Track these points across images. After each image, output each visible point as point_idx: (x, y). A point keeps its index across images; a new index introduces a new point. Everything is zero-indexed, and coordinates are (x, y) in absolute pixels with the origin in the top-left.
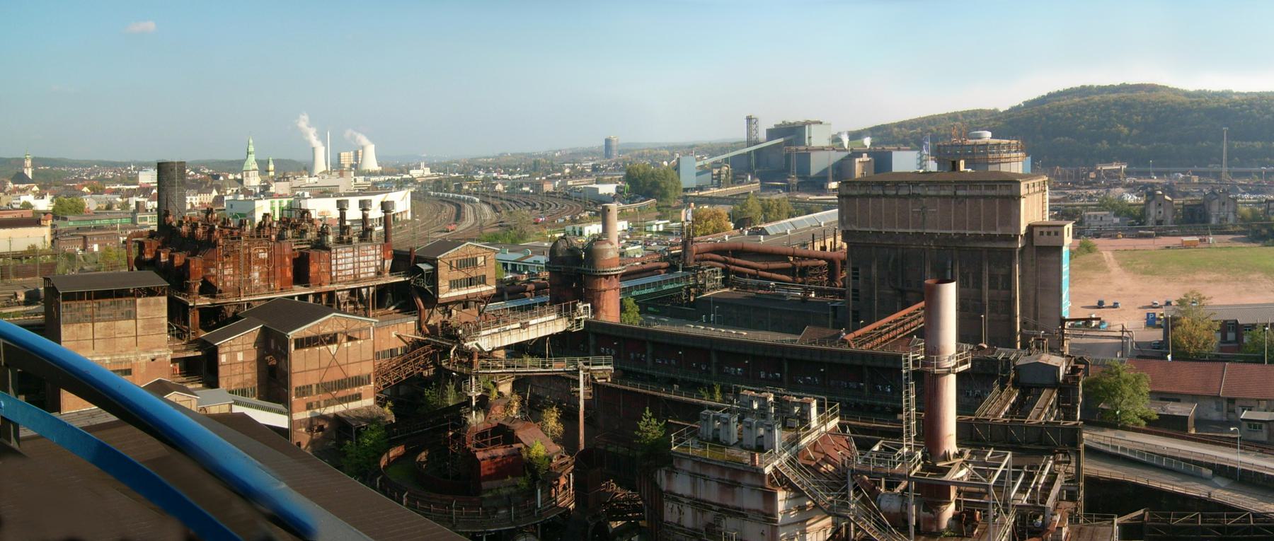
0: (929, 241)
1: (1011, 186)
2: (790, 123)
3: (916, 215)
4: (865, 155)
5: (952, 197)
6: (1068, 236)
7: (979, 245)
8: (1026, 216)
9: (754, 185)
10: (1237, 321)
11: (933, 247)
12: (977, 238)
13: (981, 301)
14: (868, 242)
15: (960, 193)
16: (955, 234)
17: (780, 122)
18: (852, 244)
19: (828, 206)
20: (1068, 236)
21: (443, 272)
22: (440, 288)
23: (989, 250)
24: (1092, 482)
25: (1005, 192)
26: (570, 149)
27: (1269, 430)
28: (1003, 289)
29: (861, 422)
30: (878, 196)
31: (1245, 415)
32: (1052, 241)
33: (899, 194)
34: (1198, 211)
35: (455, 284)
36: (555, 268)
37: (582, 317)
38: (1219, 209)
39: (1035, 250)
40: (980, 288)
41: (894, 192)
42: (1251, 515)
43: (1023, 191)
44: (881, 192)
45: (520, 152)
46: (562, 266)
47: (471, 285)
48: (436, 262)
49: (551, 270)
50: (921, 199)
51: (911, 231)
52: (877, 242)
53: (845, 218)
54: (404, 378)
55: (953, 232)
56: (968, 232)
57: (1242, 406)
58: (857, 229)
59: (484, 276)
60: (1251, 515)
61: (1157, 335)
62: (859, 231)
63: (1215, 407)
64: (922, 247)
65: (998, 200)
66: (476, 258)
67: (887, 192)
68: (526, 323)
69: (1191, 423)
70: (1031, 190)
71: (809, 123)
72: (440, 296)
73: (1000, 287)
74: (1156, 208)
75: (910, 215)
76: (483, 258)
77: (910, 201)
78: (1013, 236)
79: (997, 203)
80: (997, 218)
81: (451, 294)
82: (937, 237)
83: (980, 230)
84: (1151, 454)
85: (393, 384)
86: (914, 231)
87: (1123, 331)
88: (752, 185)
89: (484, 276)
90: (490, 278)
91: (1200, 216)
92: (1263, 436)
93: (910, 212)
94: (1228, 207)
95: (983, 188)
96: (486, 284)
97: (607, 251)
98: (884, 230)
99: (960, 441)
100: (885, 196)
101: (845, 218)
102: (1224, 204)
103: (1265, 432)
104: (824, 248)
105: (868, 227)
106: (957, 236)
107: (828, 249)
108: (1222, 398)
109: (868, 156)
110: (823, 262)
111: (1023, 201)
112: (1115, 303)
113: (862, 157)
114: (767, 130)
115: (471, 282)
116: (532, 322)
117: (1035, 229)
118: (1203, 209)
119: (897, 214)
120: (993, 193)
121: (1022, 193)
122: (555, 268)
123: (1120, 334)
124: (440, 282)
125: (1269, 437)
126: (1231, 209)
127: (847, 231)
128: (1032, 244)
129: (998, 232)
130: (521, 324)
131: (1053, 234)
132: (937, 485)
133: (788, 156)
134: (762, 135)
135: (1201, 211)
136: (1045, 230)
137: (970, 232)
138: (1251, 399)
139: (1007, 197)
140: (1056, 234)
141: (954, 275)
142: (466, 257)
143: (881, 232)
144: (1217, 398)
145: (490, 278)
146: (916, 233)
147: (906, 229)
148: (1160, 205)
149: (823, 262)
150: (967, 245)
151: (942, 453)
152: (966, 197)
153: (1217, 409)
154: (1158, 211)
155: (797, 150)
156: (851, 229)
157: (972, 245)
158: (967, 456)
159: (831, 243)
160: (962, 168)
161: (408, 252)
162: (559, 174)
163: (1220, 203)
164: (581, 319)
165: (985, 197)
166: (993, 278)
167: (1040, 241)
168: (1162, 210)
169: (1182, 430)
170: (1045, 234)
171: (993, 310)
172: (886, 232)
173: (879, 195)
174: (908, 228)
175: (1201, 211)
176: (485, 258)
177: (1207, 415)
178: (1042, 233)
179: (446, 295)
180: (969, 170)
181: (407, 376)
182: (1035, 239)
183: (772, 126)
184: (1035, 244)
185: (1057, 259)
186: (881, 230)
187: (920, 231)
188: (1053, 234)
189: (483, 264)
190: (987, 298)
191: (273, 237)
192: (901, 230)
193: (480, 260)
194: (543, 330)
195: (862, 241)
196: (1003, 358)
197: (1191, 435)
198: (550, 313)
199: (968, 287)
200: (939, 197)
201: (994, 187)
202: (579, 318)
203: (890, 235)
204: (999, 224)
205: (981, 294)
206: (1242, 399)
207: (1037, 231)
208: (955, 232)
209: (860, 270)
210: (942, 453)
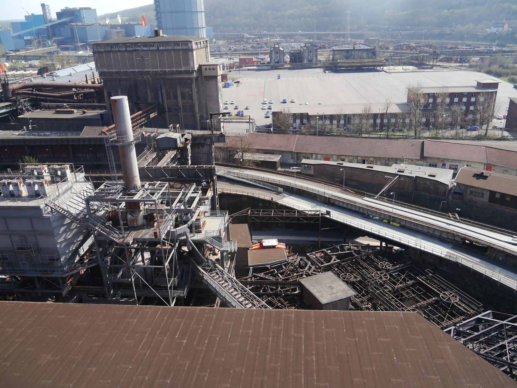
2: (70, 9)
3: (138, 61)
4: (119, 28)
8: (197, 60)
9: (53, 47)
10: (308, 113)
11: (150, 79)
12: (172, 73)
13: (178, 106)
14: (114, 78)
15: (161, 48)
16: (160, 71)
19: (83, 60)
24: (222, 196)
25: (185, 47)
27: (314, 169)
28: (189, 99)
31: (304, 161)
34: (298, 56)
38: (308, 55)
40: (177, 99)
41: (124, 49)
42: (296, 211)
44: (117, 49)
51: (136, 70)
52: (119, 77)
53: (99, 64)
55: (159, 70)
57: (304, 157)
58: (107, 71)
60: (296, 211)
61: (269, 121)
63: (291, 157)
64: (144, 79)
65: (181, 51)
67: (121, 49)
69: (278, 164)
70: (199, 46)
73: (187, 98)
74: (275, 54)
77: (134, 54)
78: (191, 71)
79: (181, 53)
82: (151, 73)
84: (255, 181)
87: (249, 119)
88: (52, 47)
91: (299, 59)
92: (312, 172)
94: (313, 54)
98: (122, 71)
99: (142, 179)
100: (119, 51)
101: (99, 64)
102: (310, 52)
103: (312, 170)
104: (94, 83)
106: (162, 72)
107: (97, 82)
108: (294, 152)
110: (92, 90)
111: (195, 52)
112: (284, 100)
113: (117, 29)
117: (202, 67)
118: (300, 55)
120: (178, 48)
123: (248, 121)
125: (314, 172)
126: (314, 55)
128: (202, 75)
129: (183, 69)
131: (212, 69)
134: (54, 16)
135: (299, 56)
136: (208, 67)
137: (168, 70)
138: (309, 153)
139: (186, 50)
140: (214, 69)
141: (163, 93)
144: (291, 152)
146: (140, 71)
148: (277, 53)
149: (92, 90)
150: (168, 77)
151: (133, 186)
152: (164, 50)
153: (292, 158)
154: (276, 56)
155: (77, 25)
156: (103, 71)
157: (170, 77)
158: (146, 186)
160: (161, 34)
163: (308, 51)
165: (174, 50)
166: (168, 94)
167: (206, 73)
168: (278, 55)
169: (274, 169)
171: (185, 111)
172: (123, 72)
175: (299, 56)
177: (287, 161)
178: (206, 69)
180: (165, 35)
182: (203, 72)
183: (59, 11)
185: (215, 82)
186: (120, 71)
188: (212, 69)
190: (181, 104)
192: (131, 70)
197: (278, 171)
199: (171, 99)
200: (150, 50)
202: (22, 290)
203: (126, 73)
205: (177, 102)
206: (304, 153)
207: (203, 68)
208: (160, 70)
209: (112, 93)
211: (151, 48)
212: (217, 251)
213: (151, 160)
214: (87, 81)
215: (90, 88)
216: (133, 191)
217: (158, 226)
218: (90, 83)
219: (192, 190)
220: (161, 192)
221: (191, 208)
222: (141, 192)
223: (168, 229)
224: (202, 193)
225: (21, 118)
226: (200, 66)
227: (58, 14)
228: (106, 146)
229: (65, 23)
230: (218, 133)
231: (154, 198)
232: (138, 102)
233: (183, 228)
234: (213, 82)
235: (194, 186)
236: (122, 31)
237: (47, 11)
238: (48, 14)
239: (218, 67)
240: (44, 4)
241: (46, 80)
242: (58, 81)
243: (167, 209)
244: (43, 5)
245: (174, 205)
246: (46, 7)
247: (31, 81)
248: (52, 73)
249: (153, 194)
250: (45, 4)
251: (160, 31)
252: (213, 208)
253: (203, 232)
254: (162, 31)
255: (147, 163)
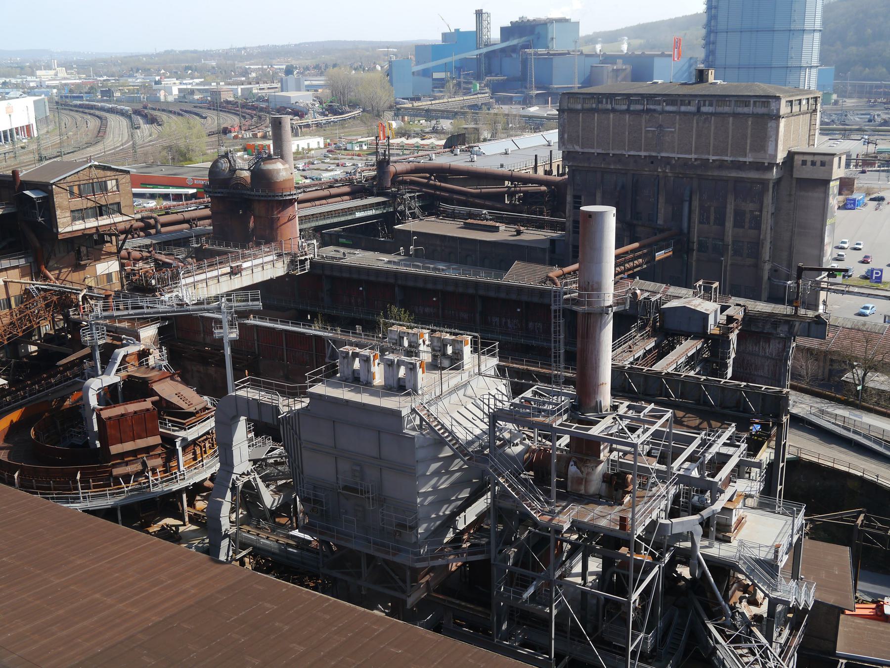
0: (665, 167)
1: (768, 102)
2: (528, 20)
3: (650, 135)
4: (619, 61)
5: (693, 114)
6: (839, 167)
7: (725, 173)
8: (785, 141)
11: (670, 175)
12: (722, 165)
14: (592, 165)
15: (705, 109)
16: (696, 159)
17: (516, 19)
18: (574, 168)
20: (839, 167)
21: (61, 199)
22: (58, 220)
23: (737, 180)
25: (761, 110)
26: (259, 47)
29: (541, 368)
30: (606, 111)
32: (818, 173)
33: (631, 109)
35: (79, 214)
36: (216, 193)
37: (307, 257)
39: (794, 182)
41: (625, 107)
43: (784, 109)
45: (192, 49)
46: (225, 191)
47: (101, 215)
48: (50, 188)
49: (211, 195)
50: (657, 115)
51: (643, 154)
53: (566, 136)
54: (20, 334)
56: (712, 158)
59: (118, 204)
62: (583, 153)
64: (656, 173)
66: (105, 182)
68: (237, 266)
71: (551, 21)
72: (60, 230)
73: (747, 225)
75: (643, 135)
76: (114, 182)
77: (645, 117)
80: (749, 141)
81: (76, 228)
83: (727, 156)
85: (6, 342)
86: (646, 154)
89: (118, 204)
90: (126, 206)
93: (643, 132)
95: (733, 103)
96: (121, 214)
97: (278, 171)
98: (611, 152)
100: (613, 110)
101: (566, 136)
105: (593, 148)
107: (555, 172)
109: (624, 63)
110: (543, 188)
111: (782, 122)
113: (615, 63)
114: (442, 34)
115: (100, 211)
116: (245, 265)
117: (796, 157)
119: (627, 133)
120: (746, 110)
121: (782, 113)
122: (216, 193)
124: (58, 212)
127: (569, 152)
128: (792, 175)
129: (749, 159)
130: (231, 268)
132: (587, 440)
133: (525, 63)
134: (495, 35)
137: (715, 158)
140: (823, 164)
141: (693, 208)
142: (91, 181)
143: (609, 154)
145: (126, 206)
146: (650, 157)
147: (638, 151)
149: (543, 188)
150: (710, 174)
151: (593, 404)
152: (712, 114)
157: (716, 173)
158: (622, 410)
159: (558, 165)
160: (711, 79)
161: (8, 176)
162: (243, 79)
164: (306, 259)
165: (735, 115)
167: (807, 173)
170: (809, 163)
172: (613, 154)
173: (608, 110)
174: (640, 150)
176: (117, 182)
178: (804, 163)
179: (69, 229)
180: (719, 82)
181: (24, 331)
182: (795, 170)
183: (507, 24)
184: (795, 176)
185: (822, 195)
187: (654, 154)
188: (818, 164)
189: (115, 189)
191: (701, 239)
192: (632, 153)
193: (111, 184)
194: (260, 274)
195: (586, 165)
196: (645, 298)
198: (267, 254)
199: (708, 223)
201: (747, 104)
202: (303, 258)
203: (619, 158)
204: (751, 150)
207: (798, 159)
208: (696, 156)
209: (583, 198)
210: (593, 404)
211: (683, 109)
212: (760, 595)
213: (641, 353)
214: (535, 168)
215: (540, 182)
216: (591, 416)
217: (633, 505)
218: (541, 172)
219: (724, 438)
220: (653, 429)
221: (716, 479)
222: (608, 421)
223: (654, 516)
224: (749, 449)
225: (399, 230)
226: (791, 155)
227: (504, 30)
228: (553, 308)
229: (514, 49)
230: (811, 314)
231: (633, 438)
232: (635, 222)
233: (688, 522)
234: (817, 194)
235: (732, 429)
236: (625, 69)
237: (485, 23)
238: (485, 31)
239: (836, 160)
240: (481, 10)
241: (458, 160)
242: (480, 164)
243: (658, 471)
244: (479, 14)
245: (676, 465)
246: (485, 16)
247: (430, 160)
248: (472, 147)
249: (633, 430)
250: (484, 12)
251: (710, 71)
252: (768, 490)
253: (734, 543)
254: (713, 71)
255: (631, 359)
